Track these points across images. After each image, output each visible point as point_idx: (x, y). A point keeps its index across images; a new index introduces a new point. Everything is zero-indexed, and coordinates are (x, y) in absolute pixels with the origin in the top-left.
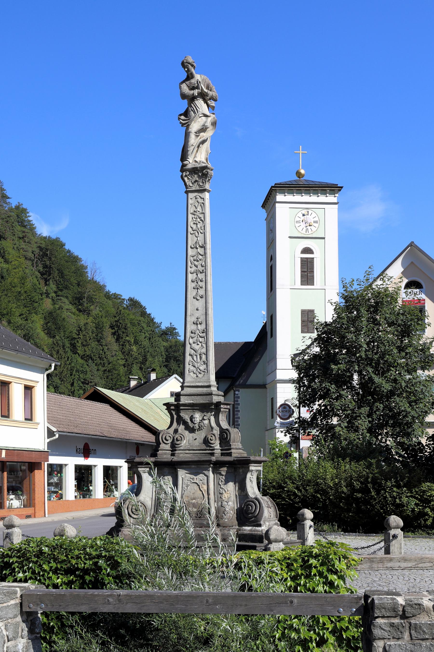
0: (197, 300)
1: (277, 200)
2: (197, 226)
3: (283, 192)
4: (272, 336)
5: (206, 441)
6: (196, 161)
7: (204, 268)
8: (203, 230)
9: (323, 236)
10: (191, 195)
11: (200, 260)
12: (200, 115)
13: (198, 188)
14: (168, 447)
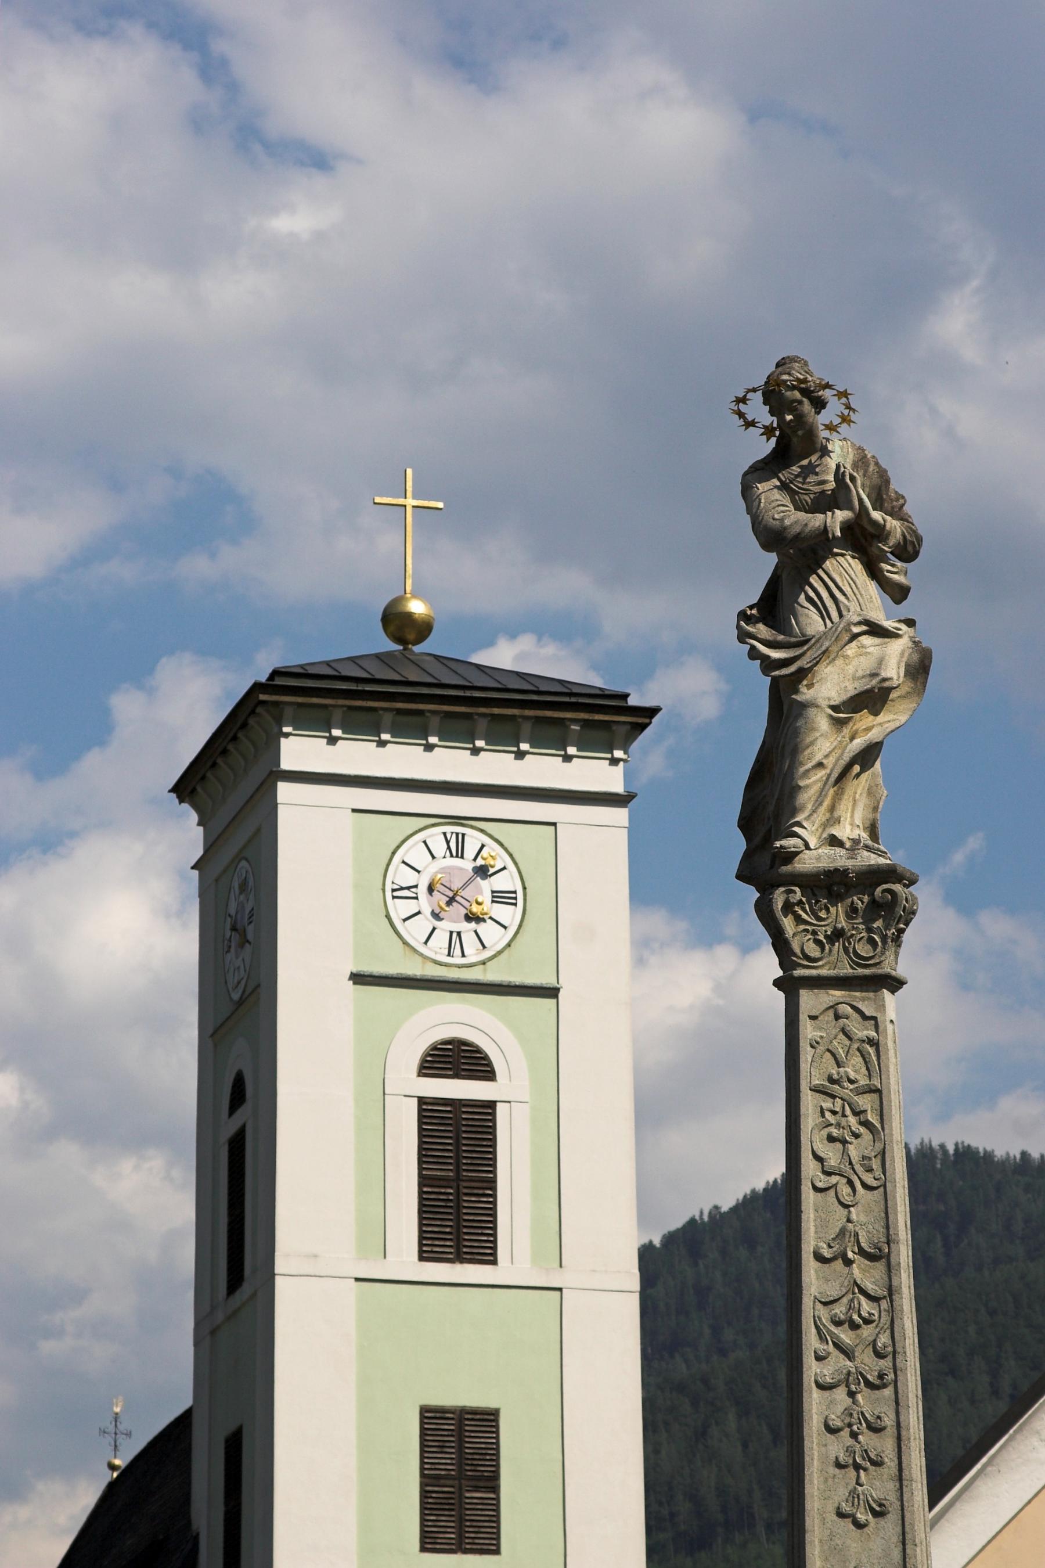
0: (859, 1526)
1: (286, 765)
2: (845, 1151)
6: (834, 841)
7: (886, 1364)
8: (878, 1173)
9: (544, 978)
10: (809, 1001)
11: (867, 1322)
12: (856, 630)
13: (845, 970)
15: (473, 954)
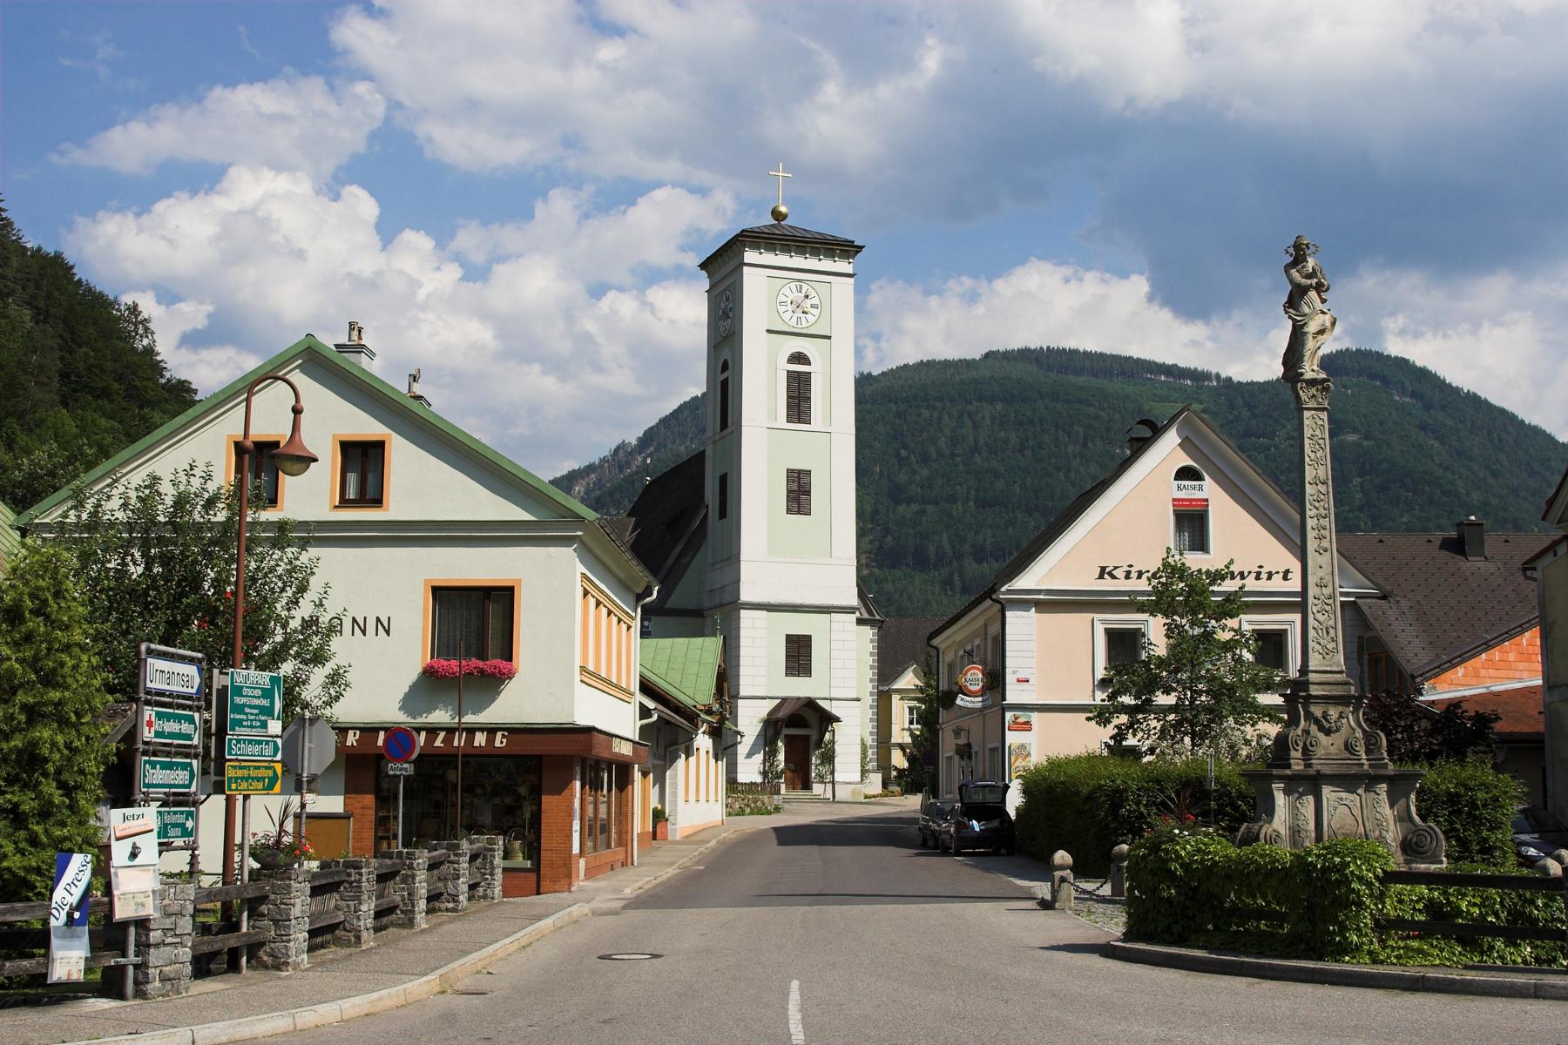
3: (756, 247)
4: (723, 514)
5: (1348, 747)
14: (1299, 755)
15: (805, 324)
